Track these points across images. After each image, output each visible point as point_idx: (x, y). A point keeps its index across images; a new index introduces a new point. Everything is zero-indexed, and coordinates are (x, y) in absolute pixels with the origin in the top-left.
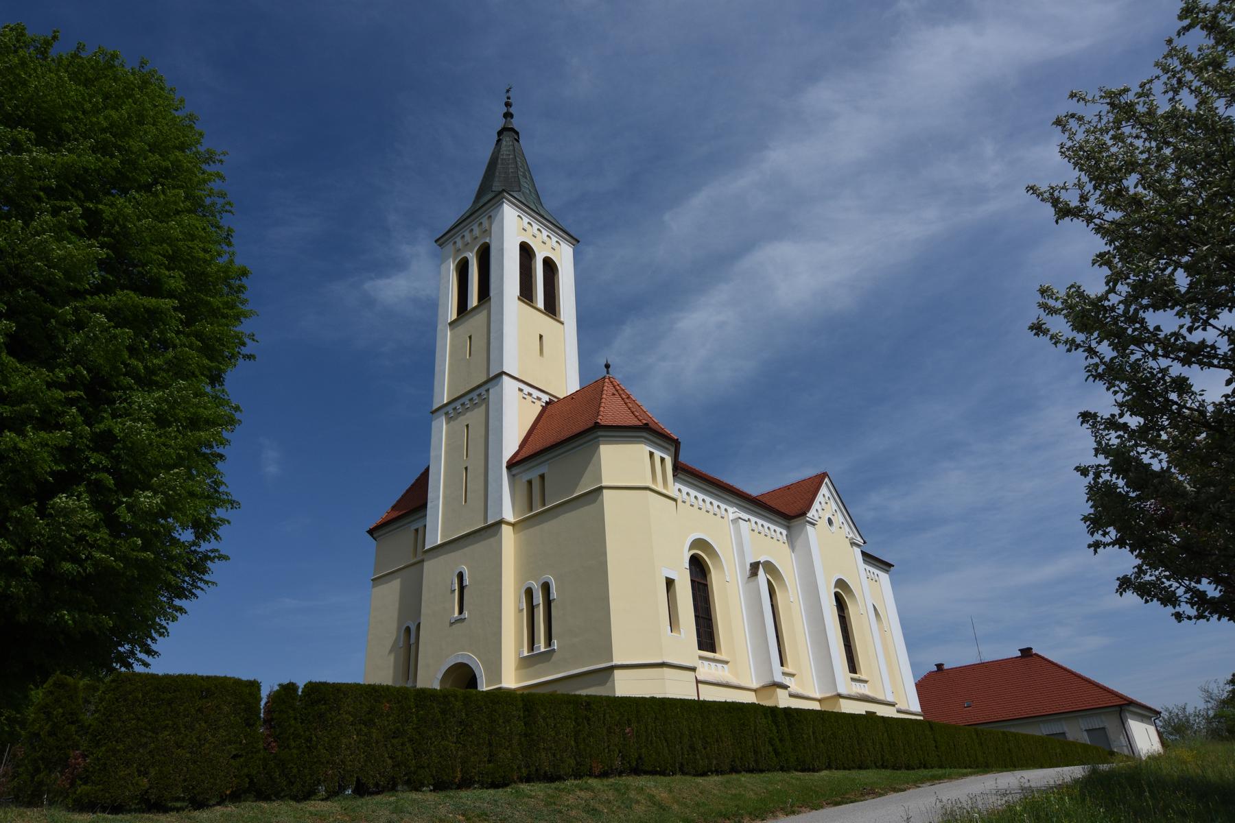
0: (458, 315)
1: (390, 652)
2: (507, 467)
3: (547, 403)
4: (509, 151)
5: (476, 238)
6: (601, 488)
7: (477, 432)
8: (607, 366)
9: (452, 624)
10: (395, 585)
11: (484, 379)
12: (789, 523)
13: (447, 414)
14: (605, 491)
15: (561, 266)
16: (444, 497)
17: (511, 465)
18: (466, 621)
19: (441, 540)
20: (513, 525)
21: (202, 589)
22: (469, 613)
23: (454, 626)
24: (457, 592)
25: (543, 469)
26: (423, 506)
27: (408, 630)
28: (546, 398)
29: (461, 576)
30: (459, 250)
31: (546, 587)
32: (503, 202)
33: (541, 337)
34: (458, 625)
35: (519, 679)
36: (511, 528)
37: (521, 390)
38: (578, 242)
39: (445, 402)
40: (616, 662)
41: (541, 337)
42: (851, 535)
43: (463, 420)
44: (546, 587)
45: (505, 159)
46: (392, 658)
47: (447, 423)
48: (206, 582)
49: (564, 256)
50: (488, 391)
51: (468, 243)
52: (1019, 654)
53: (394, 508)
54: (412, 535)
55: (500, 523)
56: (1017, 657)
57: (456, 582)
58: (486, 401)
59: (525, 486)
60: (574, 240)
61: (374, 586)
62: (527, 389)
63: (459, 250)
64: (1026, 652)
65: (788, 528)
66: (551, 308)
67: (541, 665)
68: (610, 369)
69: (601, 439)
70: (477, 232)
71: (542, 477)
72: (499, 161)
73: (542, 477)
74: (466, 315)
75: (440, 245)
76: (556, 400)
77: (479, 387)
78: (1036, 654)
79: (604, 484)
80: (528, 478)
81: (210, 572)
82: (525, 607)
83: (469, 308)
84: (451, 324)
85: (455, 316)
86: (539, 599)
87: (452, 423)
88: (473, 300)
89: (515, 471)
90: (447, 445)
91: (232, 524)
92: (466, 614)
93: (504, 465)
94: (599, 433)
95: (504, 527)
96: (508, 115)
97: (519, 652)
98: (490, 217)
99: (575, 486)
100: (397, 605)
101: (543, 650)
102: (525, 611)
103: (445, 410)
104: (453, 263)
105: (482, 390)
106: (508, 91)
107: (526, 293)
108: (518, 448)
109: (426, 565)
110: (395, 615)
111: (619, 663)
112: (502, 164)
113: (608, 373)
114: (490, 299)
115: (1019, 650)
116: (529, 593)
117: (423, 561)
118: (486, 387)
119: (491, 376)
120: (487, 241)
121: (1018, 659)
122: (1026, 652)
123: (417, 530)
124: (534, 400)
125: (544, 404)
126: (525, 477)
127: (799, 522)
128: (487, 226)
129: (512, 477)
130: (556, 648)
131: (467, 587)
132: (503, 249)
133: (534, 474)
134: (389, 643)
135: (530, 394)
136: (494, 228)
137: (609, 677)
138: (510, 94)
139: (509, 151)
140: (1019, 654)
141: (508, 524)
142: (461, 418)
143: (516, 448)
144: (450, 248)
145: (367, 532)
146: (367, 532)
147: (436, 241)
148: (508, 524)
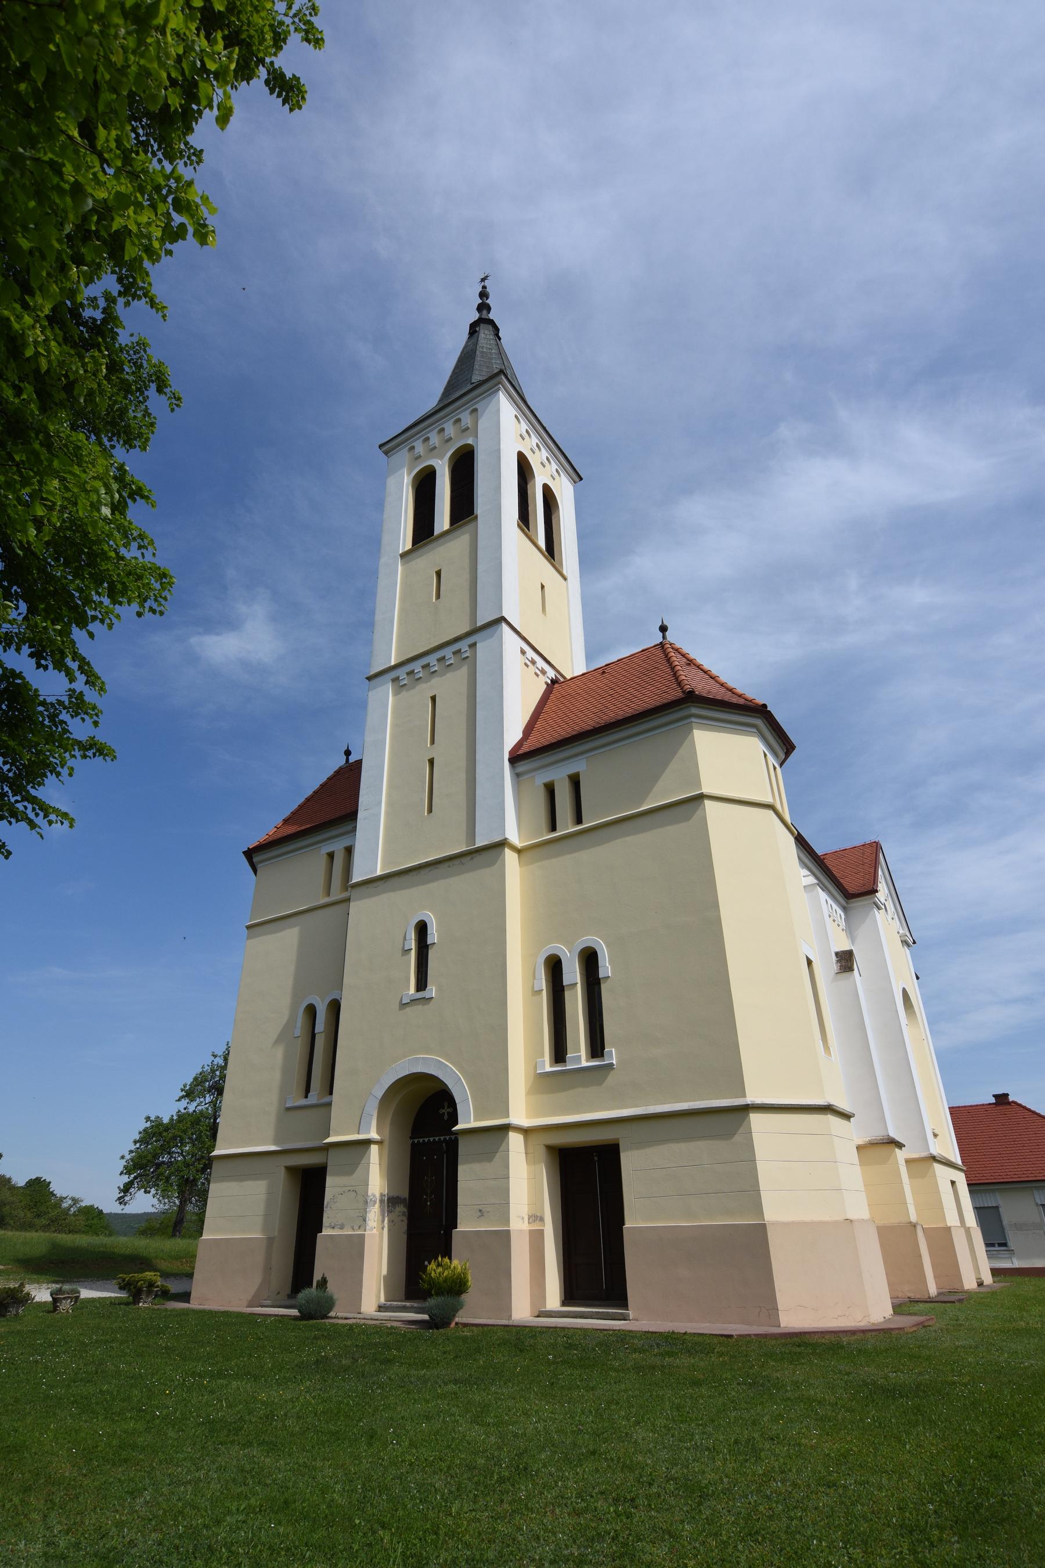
0: (413, 545)
1: (277, 1042)
2: (510, 760)
3: (552, 680)
4: (490, 344)
5: (451, 439)
6: (701, 797)
7: (452, 707)
8: (663, 629)
9: (403, 1006)
10: (290, 937)
11: (466, 628)
12: (847, 903)
13: (396, 680)
14: (707, 803)
15: (562, 503)
16: (390, 804)
17: (516, 758)
18: (433, 1000)
19: (382, 869)
20: (519, 851)
21: (32, 825)
22: (440, 989)
23: (408, 1010)
24: (413, 953)
25: (572, 768)
26: (351, 816)
27: (311, 1010)
28: (551, 674)
29: (422, 929)
30: (418, 457)
31: (590, 959)
32: (499, 389)
33: (543, 587)
34: (418, 1008)
35: (532, 1113)
36: (516, 855)
37: (523, 652)
38: (581, 479)
39: (393, 663)
40: (751, 1098)
41: (543, 587)
42: (901, 931)
43: (425, 690)
44: (590, 959)
45: (486, 353)
46: (279, 1052)
47: (395, 694)
48: (45, 809)
49: (565, 492)
50: (473, 646)
51: (435, 448)
52: (993, 1100)
53: (286, 821)
54: (324, 860)
55: (503, 844)
56: (990, 1104)
57: (413, 937)
58: (471, 662)
59: (541, 796)
60: (577, 476)
61: (249, 938)
62: (530, 654)
63: (418, 457)
64: (1002, 1099)
65: (845, 909)
66: (551, 550)
67: (581, 1090)
68: (667, 633)
69: (693, 720)
70: (450, 429)
71: (575, 782)
72: (478, 353)
73: (575, 782)
74: (431, 541)
75: (386, 453)
76: (562, 680)
77: (457, 640)
78: (1013, 1102)
79: (706, 790)
80: (547, 780)
81: (65, 772)
82: (544, 987)
83: (437, 532)
84: (403, 556)
85: (409, 546)
86: (573, 974)
87: (404, 693)
88: (443, 519)
89: (522, 767)
90: (394, 725)
91: (85, 722)
92: (432, 990)
93: (506, 756)
94: (694, 711)
95: (508, 852)
96: (483, 307)
97: (533, 1061)
98: (476, 410)
99: (644, 794)
100: (292, 969)
101: (585, 1063)
102: (544, 993)
103: (393, 674)
104: (409, 474)
105: (463, 645)
106: (483, 280)
107: (525, 517)
108: (521, 736)
109: (354, 906)
110: (289, 983)
111: (759, 1100)
112: (482, 357)
113: (664, 637)
114: (476, 517)
115: (994, 1096)
116: (554, 966)
117: (347, 900)
118: (470, 640)
119: (479, 624)
120: (470, 441)
121: (992, 1106)
122: (1002, 1099)
123: (331, 856)
124: (539, 672)
125: (549, 682)
126: (542, 778)
127: (860, 904)
128: (469, 421)
129: (517, 776)
130: (614, 1062)
131: (435, 947)
132: (499, 451)
133: (559, 775)
134: (274, 1030)
135: (533, 662)
136: (483, 424)
137: (744, 1120)
138: (486, 283)
139: (490, 344)
140: (993, 1100)
141: (514, 848)
142: (422, 686)
143: (519, 735)
144: (403, 455)
145: (244, 853)
146: (244, 853)
147: (381, 446)
148: (514, 848)
